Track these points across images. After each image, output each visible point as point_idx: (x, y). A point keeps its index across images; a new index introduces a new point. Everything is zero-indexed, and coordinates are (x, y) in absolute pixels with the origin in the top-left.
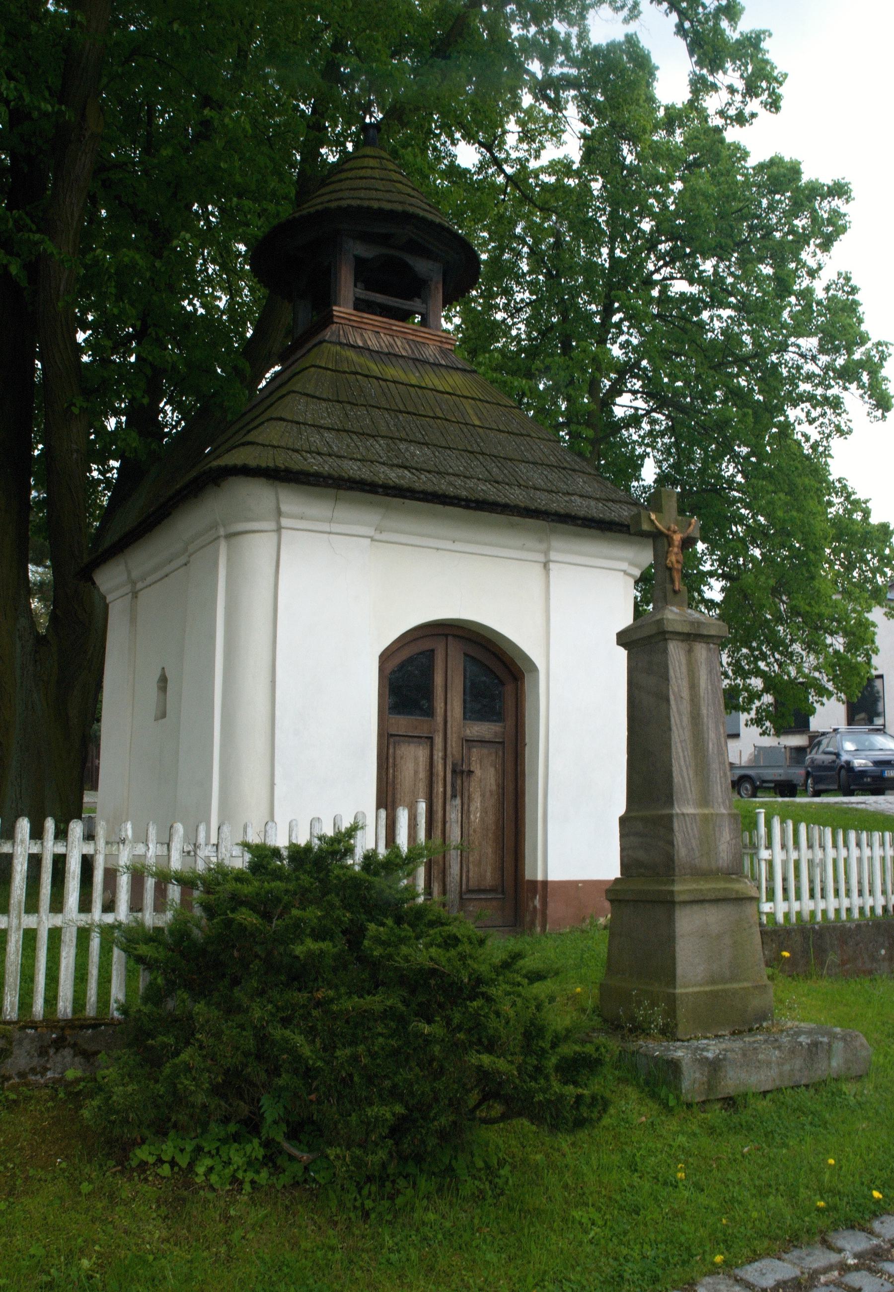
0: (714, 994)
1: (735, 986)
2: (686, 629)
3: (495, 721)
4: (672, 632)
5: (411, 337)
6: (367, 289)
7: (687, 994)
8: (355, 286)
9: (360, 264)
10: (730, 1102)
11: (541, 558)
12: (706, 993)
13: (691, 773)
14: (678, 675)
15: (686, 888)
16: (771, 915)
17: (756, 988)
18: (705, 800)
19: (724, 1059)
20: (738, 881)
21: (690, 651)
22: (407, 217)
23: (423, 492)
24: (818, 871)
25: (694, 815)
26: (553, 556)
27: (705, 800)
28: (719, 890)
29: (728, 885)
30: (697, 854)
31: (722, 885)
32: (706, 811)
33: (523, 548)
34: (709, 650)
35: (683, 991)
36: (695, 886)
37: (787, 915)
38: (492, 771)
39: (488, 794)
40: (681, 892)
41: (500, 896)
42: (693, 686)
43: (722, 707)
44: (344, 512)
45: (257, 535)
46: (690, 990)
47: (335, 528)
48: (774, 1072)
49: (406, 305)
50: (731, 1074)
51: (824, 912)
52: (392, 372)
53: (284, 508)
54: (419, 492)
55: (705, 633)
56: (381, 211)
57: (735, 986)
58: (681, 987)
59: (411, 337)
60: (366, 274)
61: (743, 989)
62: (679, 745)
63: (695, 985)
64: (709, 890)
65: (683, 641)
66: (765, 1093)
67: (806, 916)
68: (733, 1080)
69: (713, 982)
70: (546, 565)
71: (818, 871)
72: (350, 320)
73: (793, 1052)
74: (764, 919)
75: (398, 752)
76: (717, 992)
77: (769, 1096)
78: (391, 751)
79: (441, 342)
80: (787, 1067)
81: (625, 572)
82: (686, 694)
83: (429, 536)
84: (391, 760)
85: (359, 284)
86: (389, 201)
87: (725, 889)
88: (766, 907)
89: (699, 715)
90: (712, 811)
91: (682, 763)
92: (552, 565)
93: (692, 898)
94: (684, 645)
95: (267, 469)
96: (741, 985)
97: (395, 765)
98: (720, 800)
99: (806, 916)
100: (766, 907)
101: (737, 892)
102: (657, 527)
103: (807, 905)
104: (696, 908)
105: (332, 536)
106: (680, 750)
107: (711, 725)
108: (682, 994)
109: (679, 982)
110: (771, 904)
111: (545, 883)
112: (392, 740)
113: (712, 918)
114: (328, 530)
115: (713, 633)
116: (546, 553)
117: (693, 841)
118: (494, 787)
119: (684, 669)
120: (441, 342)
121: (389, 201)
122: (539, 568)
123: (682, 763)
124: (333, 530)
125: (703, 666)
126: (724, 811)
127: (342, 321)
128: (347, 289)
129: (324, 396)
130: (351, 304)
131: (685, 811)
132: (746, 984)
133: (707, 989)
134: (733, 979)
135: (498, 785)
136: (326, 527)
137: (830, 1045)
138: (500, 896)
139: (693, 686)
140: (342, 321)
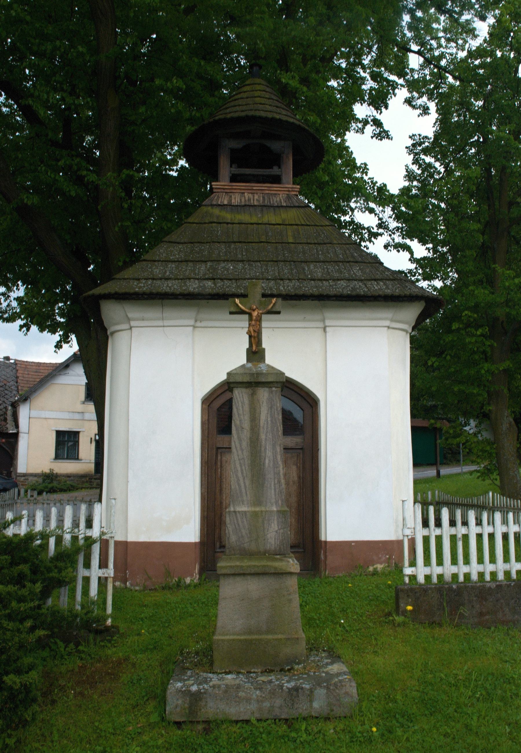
0: (250, 642)
1: (270, 637)
2: (246, 379)
3: (298, 435)
4: (234, 383)
5: (267, 192)
6: (239, 167)
7: (223, 640)
8: (231, 167)
9: (233, 151)
10: (209, 726)
11: (321, 325)
12: (240, 640)
13: (248, 483)
14: (241, 412)
15: (229, 564)
16: (413, 577)
17: (288, 639)
18: (258, 501)
19: (205, 693)
20: (281, 560)
21: (253, 394)
22: (254, 119)
23: (210, 295)
24: (460, 544)
25: (245, 512)
26: (328, 323)
27: (258, 501)
28: (258, 566)
29: (270, 563)
30: (246, 540)
31: (264, 563)
32: (257, 509)
33: (304, 320)
34: (272, 392)
35: (220, 637)
36: (238, 563)
37: (428, 578)
38: (294, 468)
39: (291, 483)
40: (222, 567)
41: (302, 550)
42: (254, 419)
43: (281, 432)
44: (169, 312)
45: (121, 333)
46: (227, 637)
47: (166, 323)
48: (253, 706)
49: (275, 171)
50: (211, 704)
51: (493, 574)
52: (245, 217)
53: (130, 315)
54: (206, 295)
55: (263, 380)
56: (232, 119)
57: (270, 637)
58: (220, 634)
59: (267, 192)
60: (238, 158)
61: (276, 639)
62: (237, 463)
63: (234, 634)
64: (249, 566)
65: (246, 387)
66: (237, 722)
67: (448, 577)
68: (212, 709)
69: (250, 633)
70: (325, 329)
71: (460, 544)
72: (224, 189)
73: (273, 694)
74: (407, 580)
75: (224, 459)
76: (251, 640)
77: (239, 725)
78: (219, 458)
79: (289, 191)
80: (267, 704)
81: (389, 327)
82: (247, 425)
83: (215, 320)
84: (219, 464)
85: (233, 166)
86: (242, 111)
87: (264, 566)
88: (408, 571)
89: (258, 439)
90: (263, 509)
91: (240, 474)
92: (328, 329)
93: (233, 572)
94: (249, 391)
95: (116, 293)
96: (276, 637)
97: (221, 466)
98: (273, 501)
99: (448, 577)
100: (408, 571)
101: (276, 568)
102: (241, 309)
103: (448, 569)
104: (238, 579)
105: (165, 328)
106: (238, 466)
107: (269, 447)
108: (218, 640)
109: (218, 631)
110: (413, 569)
111: (326, 542)
112: (220, 451)
113: (254, 587)
114: (161, 324)
115: (270, 379)
116: (323, 321)
117: (243, 531)
118: (296, 479)
119: (247, 407)
120: (289, 191)
121: (242, 111)
122: (320, 331)
123: (240, 474)
124: (165, 324)
125: (265, 404)
126: (275, 509)
127: (219, 191)
128: (225, 169)
129: (182, 241)
130: (228, 179)
131: (238, 509)
132: (280, 636)
133: (242, 637)
134: (268, 632)
135: (299, 477)
136: (160, 323)
137: (311, 691)
138: (302, 550)
139: (254, 419)
140: (219, 191)
